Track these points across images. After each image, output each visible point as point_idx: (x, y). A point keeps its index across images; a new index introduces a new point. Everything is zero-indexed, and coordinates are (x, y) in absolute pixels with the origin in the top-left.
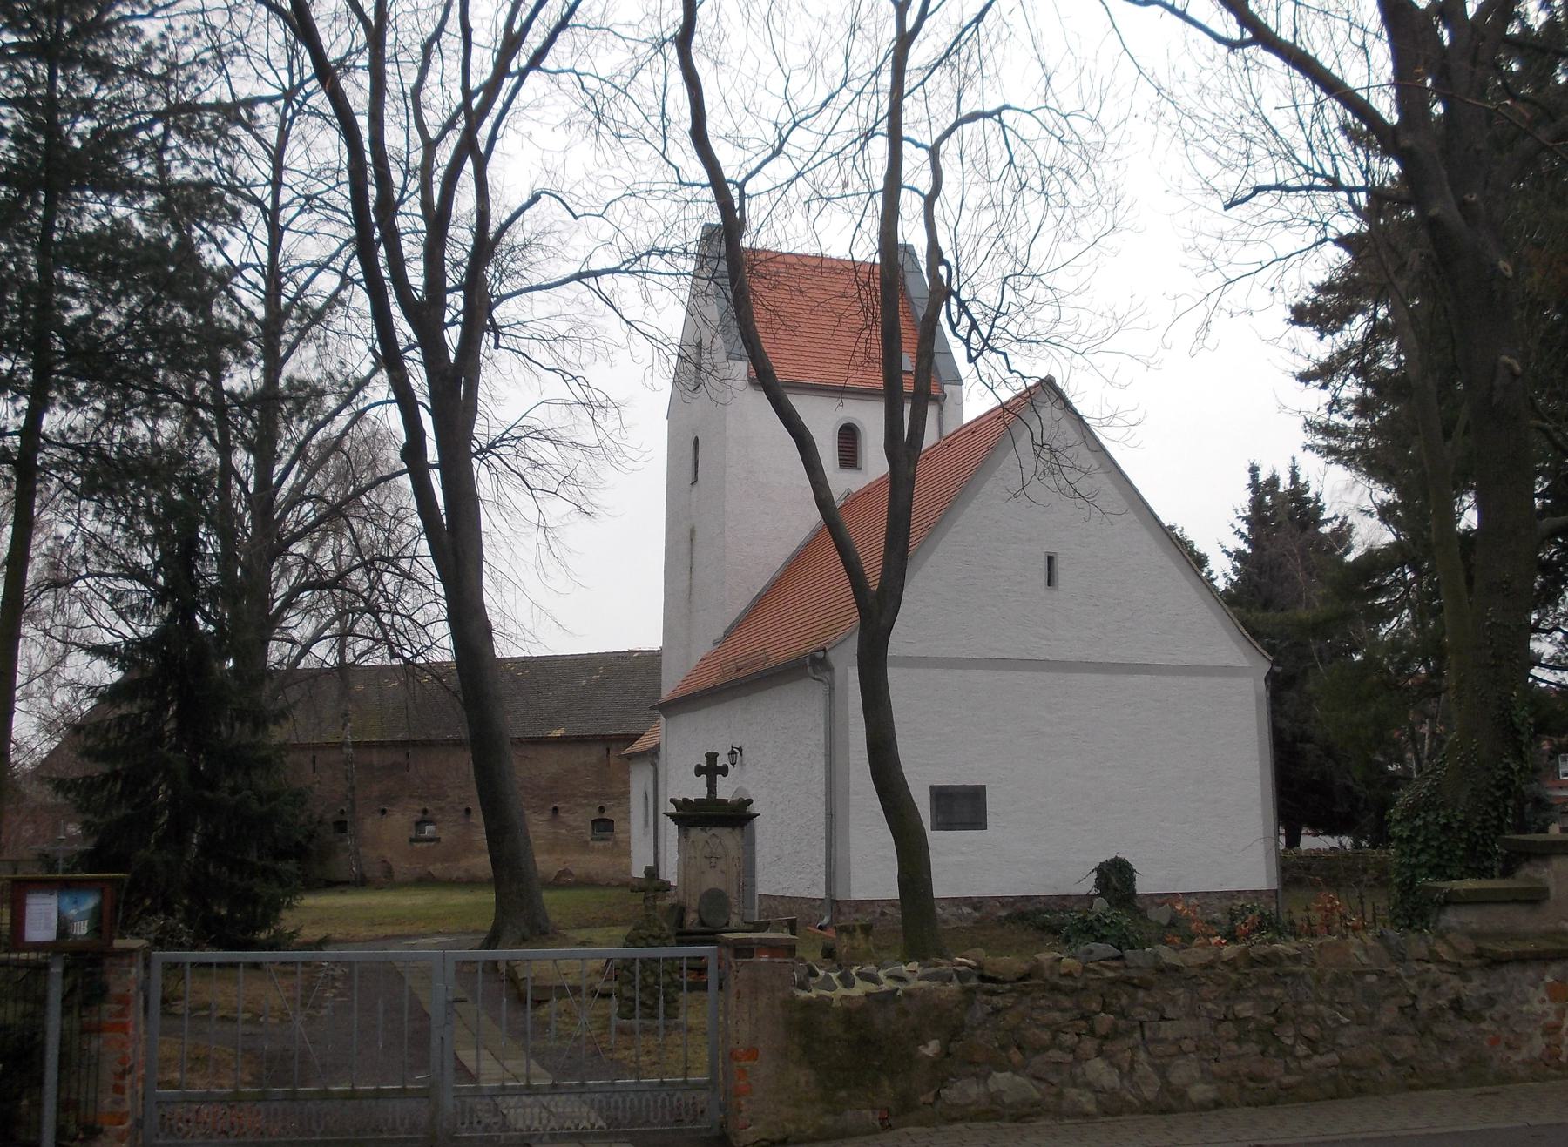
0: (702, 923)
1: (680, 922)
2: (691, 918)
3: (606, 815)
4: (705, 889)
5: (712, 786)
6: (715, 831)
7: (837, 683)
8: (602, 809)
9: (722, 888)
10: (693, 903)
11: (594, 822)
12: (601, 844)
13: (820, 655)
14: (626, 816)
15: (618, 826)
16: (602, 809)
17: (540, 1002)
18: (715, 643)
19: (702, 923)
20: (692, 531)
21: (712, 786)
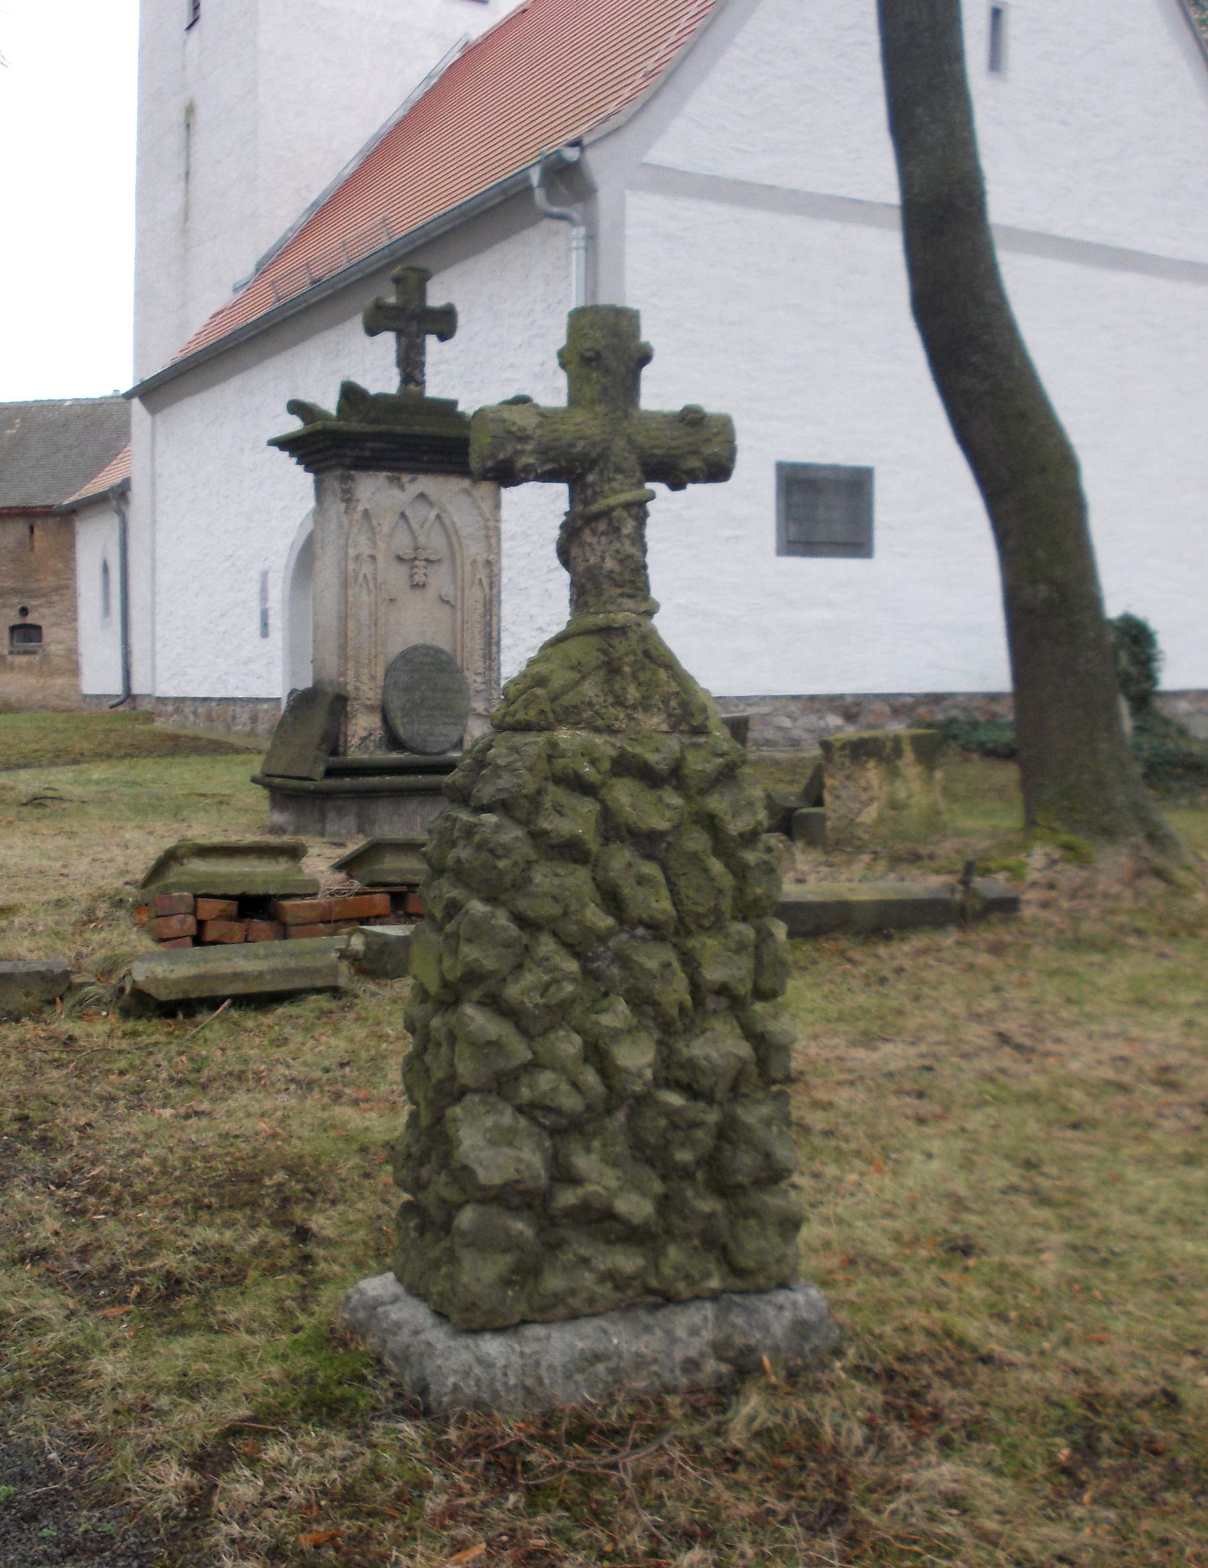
0: (393, 741)
1: (333, 743)
2: (362, 727)
3: (31, 619)
4: (396, 647)
5: (411, 364)
6: (426, 484)
7: (604, 225)
8: (24, 611)
9: (443, 642)
10: (366, 686)
11: (13, 629)
12: (23, 659)
13: (572, 154)
14: (71, 615)
15: (49, 634)
16: (24, 611)
17: (1141, 1002)
18: (236, 290)
19: (393, 741)
20: (190, 110)
21: (411, 364)
